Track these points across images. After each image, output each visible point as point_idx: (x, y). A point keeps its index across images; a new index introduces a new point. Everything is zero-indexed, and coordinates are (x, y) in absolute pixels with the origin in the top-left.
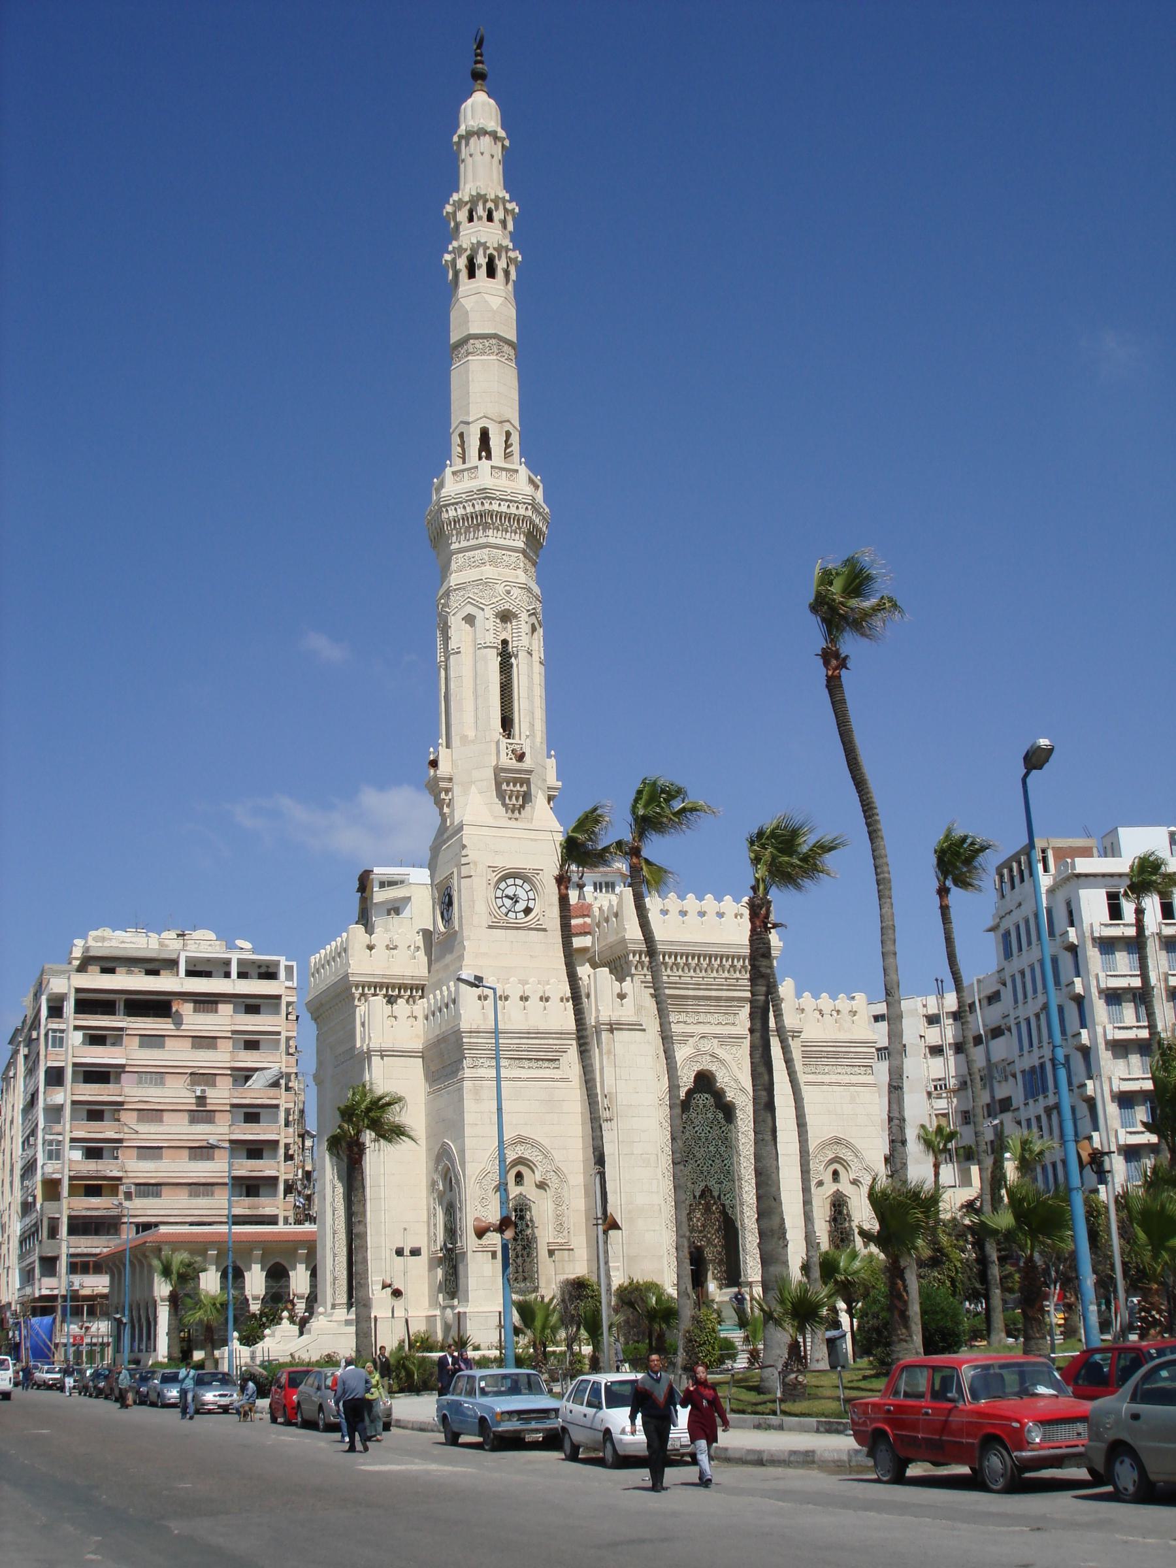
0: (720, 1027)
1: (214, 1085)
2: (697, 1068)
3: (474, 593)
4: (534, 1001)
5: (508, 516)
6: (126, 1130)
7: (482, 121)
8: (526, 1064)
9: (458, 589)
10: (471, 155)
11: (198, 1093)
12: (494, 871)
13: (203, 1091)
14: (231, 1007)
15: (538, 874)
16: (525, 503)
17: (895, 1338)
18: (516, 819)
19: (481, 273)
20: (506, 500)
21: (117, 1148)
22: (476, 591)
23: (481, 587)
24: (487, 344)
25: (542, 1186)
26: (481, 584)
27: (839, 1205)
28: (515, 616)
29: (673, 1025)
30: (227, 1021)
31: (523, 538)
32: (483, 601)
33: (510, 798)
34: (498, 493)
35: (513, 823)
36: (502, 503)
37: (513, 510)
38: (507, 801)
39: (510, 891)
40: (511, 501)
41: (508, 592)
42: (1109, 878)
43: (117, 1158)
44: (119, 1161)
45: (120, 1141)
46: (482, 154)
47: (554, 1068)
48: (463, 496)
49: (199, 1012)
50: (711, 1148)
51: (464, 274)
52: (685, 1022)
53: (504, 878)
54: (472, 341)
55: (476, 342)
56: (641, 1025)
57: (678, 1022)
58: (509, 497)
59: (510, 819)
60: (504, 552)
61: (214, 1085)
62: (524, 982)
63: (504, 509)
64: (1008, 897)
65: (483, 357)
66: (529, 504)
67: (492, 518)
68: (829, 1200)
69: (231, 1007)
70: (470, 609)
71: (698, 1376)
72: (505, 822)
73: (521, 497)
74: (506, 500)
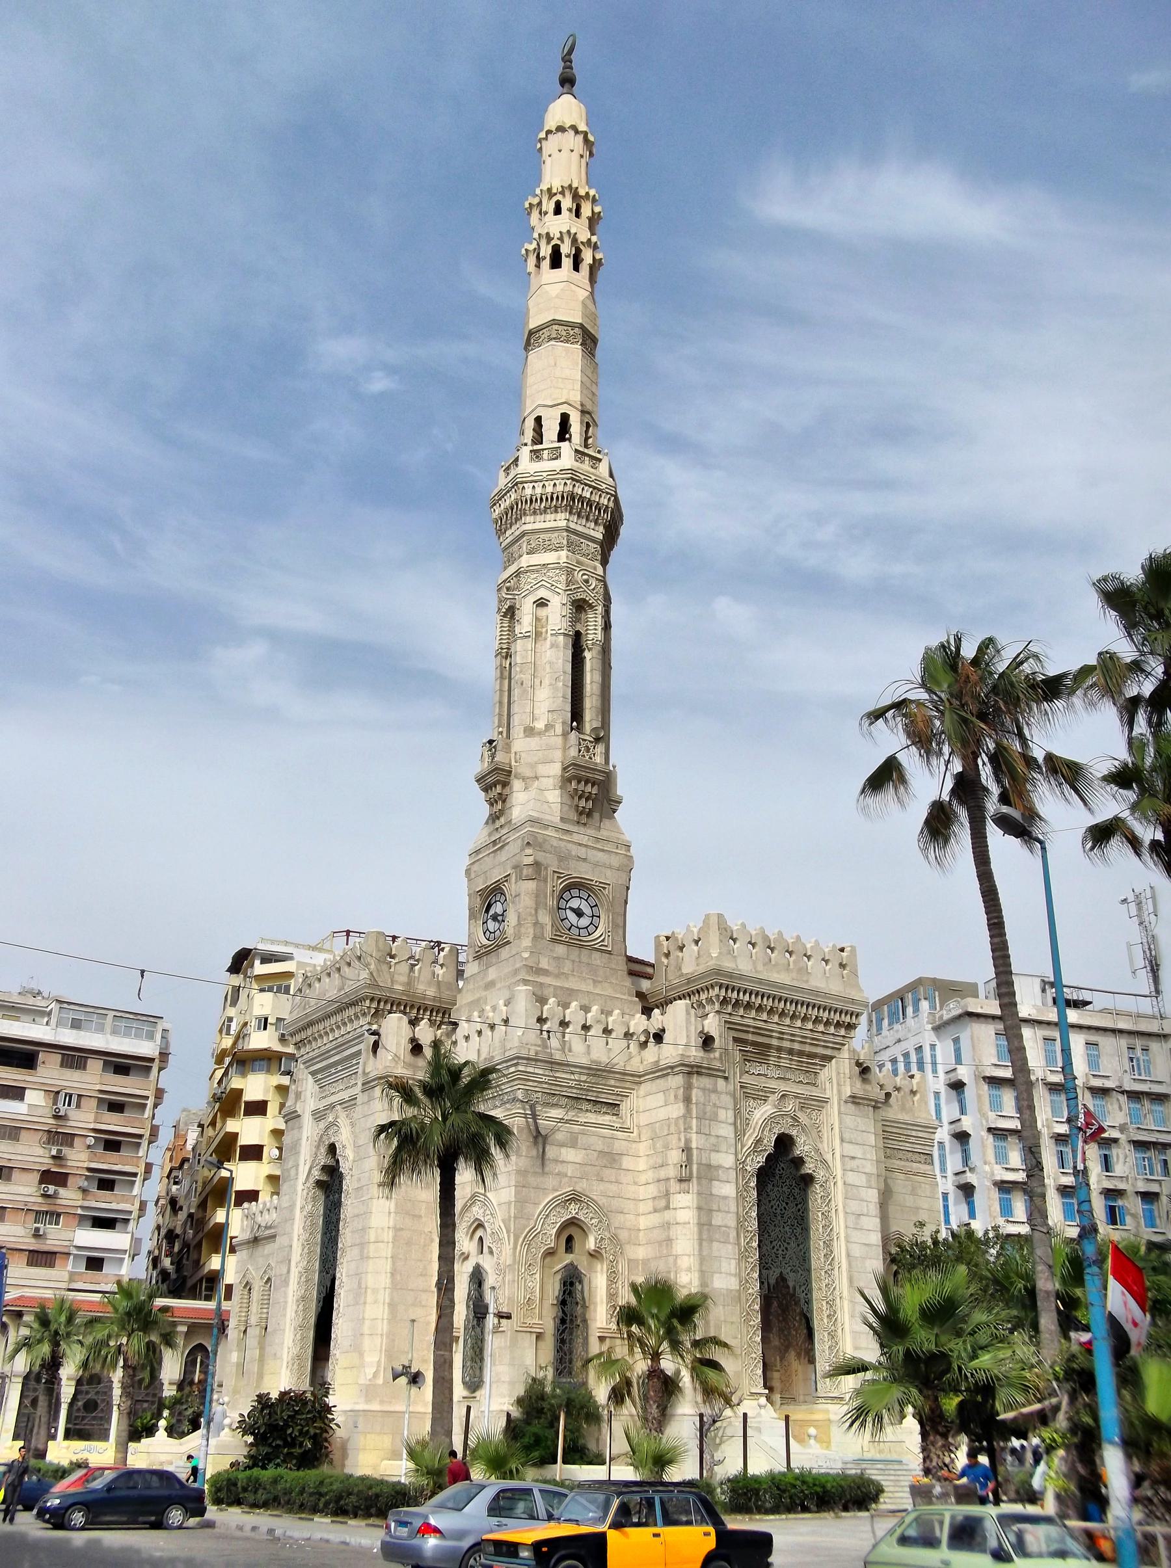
0: (801, 1086)
1: (71, 1145)
2: (777, 1131)
3: (549, 576)
4: (596, 1031)
8: (585, 1106)
11: (54, 1153)
13: (59, 1151)
15: (604, 888)
16: (608, 493)
17: (790, 1476)
19: (567, 263)
20: (590, 486)
23: (558, 571)
24: (572, 333)
25: (595, 1255)
27: (572, 1284)
28: (591, 606)
30: (97, 1079)
31: (601, 529)
34: (583, 477)
39: (575, 903)
40: (594, 488)
41: (587, 581)
42: (1163, 974)
47: (614, 1115)
48: (545, 474)
49: (66, 1067)
50: (787, 1229)
51: (546, 264)
52: (765, 1075)
53: (568, 888)
54: (556, 327)
55: (561, 328)
57: (759, 1074)
58: (593, 484)
60: (582, 540)
61: (71, 1145)
62: (586, 1009)
64: (885, 1032)
65: (566, 345)
66: (612, 495)
67: (574, 502)
68: (559, 1277)
70: (542, 593)
73: (604, 486)
74: (590, 486)
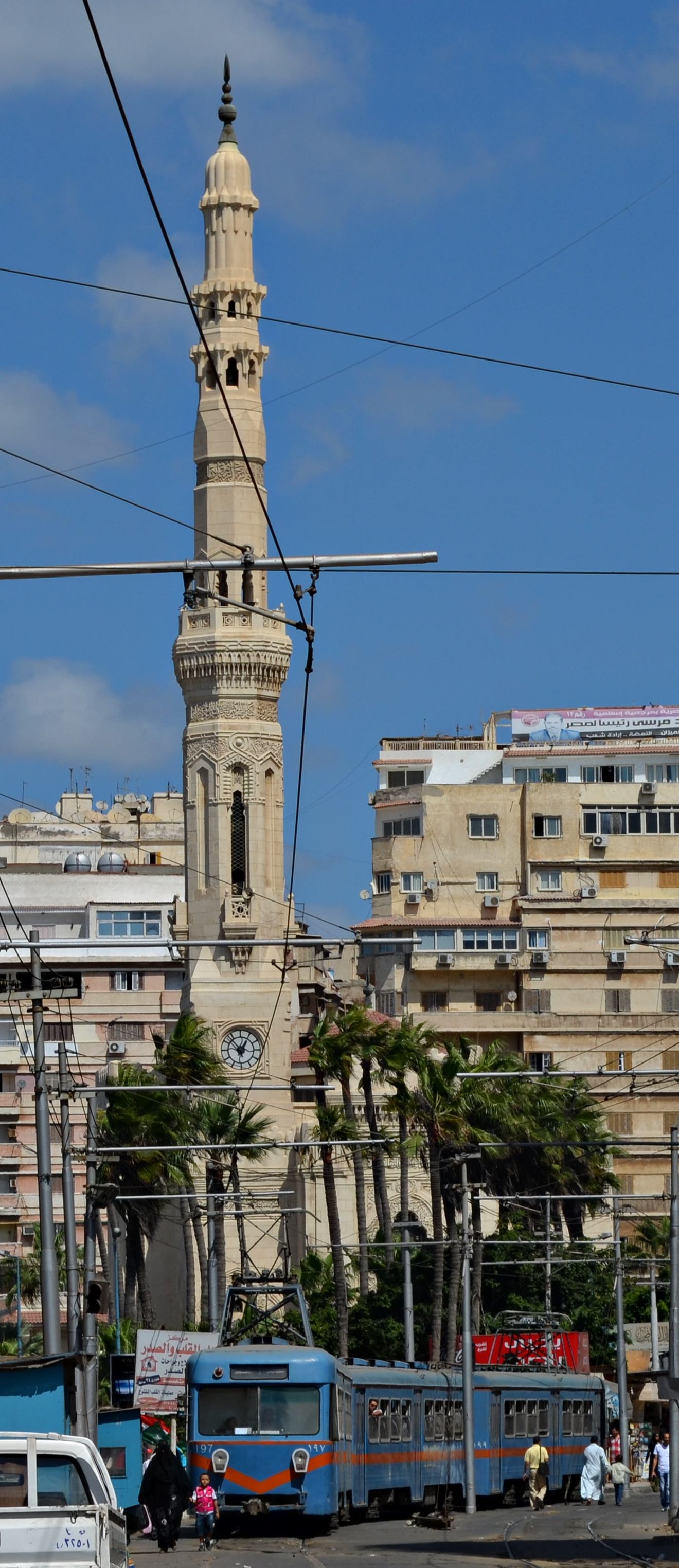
5: (239, 666)
6: (24, 1152)
7: (237, 193)
9: (195, 741)
10: (224, 232)
12: (220, 1026)
14: (161, 978)
16: (256, 651)
18: (243, 973)
21: (14, 1177)
22: (208, 745)
23: (213, 741)
26: (213, 738)
28: (247, 768)
29: (387, 1170)
32: (214, 756)
33: (237, 953)
35: (240, 977)
36: (232, 654)
37: (244, 660)
38: (235, 958)
43: (14, 1190)
44: (17, 1194)
45: (15, 1167)
46: (236, 232)
56: (342, 1172)
58: (239, 647)
59: (237, 973)
63: (235, 660)
69: (161, 978)
71: (203, 1481)
72: (232, 978)
